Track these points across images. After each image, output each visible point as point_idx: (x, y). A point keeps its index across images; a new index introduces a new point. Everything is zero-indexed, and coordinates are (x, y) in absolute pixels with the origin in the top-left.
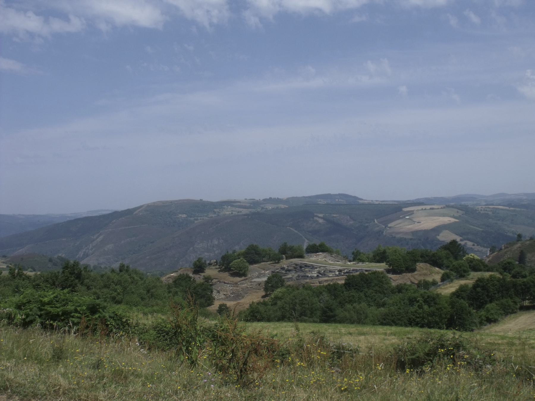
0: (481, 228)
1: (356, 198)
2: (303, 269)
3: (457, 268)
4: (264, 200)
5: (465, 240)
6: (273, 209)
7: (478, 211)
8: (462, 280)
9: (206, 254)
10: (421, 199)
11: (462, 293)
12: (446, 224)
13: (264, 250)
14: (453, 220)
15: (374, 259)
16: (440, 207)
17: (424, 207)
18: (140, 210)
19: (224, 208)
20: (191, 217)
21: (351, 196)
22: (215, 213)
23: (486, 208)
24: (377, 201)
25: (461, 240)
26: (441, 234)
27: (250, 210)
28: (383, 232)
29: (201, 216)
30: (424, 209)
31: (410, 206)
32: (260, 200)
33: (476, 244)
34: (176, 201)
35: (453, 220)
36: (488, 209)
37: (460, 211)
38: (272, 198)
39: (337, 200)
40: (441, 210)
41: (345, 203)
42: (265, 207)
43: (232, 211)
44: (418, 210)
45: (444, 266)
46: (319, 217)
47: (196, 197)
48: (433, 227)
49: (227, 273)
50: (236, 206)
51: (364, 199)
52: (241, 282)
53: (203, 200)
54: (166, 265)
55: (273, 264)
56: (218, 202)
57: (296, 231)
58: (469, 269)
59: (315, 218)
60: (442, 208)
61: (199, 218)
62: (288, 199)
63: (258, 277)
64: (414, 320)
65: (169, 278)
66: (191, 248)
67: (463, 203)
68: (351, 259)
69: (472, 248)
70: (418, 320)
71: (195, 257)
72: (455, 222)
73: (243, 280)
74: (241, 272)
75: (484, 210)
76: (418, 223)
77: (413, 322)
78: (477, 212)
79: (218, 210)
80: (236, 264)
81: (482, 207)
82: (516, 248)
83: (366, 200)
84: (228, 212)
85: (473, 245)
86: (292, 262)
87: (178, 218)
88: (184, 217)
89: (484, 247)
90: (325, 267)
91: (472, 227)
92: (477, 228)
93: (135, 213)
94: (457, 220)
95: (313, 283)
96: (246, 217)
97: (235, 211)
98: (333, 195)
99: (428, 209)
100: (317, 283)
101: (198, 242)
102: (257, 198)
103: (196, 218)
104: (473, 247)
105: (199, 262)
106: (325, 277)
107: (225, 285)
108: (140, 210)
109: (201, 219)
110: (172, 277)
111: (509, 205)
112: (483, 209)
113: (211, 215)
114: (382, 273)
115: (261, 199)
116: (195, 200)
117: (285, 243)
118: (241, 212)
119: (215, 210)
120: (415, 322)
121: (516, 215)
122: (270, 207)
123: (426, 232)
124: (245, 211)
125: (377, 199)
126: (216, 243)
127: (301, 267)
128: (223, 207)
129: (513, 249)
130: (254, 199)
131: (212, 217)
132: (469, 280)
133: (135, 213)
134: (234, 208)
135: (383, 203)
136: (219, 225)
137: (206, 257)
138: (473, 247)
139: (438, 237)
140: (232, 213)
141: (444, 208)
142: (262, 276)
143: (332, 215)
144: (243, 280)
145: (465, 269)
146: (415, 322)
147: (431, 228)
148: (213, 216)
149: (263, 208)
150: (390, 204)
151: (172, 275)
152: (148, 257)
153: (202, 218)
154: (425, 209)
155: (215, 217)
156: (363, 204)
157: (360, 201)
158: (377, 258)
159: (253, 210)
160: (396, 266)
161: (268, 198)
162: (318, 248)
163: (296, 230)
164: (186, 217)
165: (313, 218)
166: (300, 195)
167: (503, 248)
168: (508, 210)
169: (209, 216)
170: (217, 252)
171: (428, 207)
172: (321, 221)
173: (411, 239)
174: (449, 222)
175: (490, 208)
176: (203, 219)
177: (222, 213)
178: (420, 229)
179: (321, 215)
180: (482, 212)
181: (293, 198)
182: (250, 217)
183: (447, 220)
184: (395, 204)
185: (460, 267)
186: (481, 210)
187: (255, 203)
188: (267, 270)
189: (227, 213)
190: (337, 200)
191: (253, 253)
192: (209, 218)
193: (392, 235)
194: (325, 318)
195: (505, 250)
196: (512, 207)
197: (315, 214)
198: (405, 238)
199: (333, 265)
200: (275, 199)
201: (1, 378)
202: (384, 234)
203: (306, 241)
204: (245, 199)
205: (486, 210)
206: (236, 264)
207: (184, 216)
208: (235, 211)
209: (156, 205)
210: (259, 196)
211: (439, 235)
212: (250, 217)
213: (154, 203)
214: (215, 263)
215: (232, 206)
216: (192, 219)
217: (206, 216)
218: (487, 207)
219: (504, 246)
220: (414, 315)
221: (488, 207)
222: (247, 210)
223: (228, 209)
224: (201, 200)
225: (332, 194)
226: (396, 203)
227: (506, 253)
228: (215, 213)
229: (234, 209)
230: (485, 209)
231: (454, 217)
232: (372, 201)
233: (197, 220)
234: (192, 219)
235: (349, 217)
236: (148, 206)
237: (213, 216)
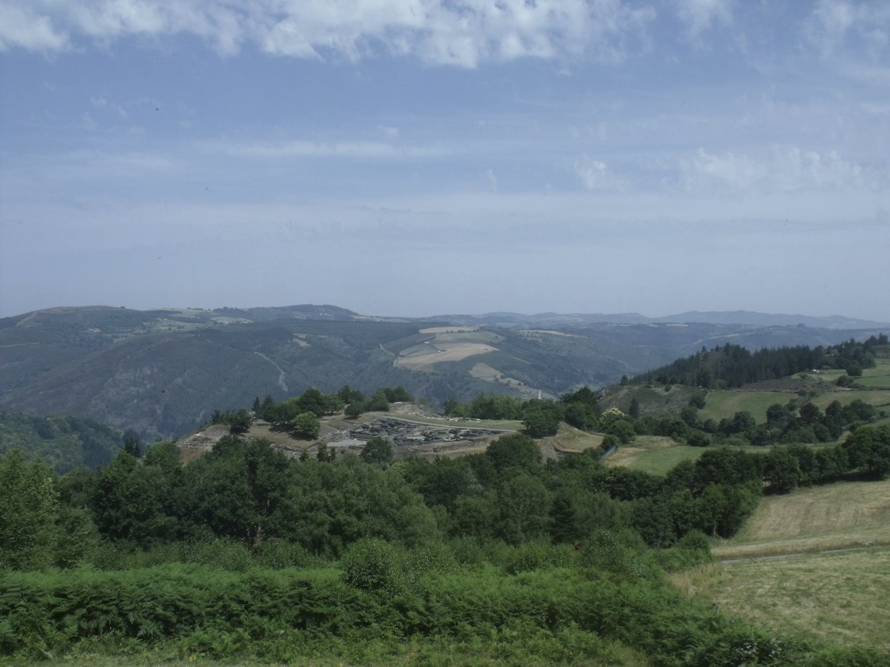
0: (528, 361)
1: (348, 312)
2: (395, 428)
3: (619, 430)
4: (217, 310)
5: (508, 377)
6: (232, 324)
7: (524, 336)
8: (626, 447)
9: (132, 388)
10: (439, 316)
11: (687, 471)
12: (481, 353)
13: (326, 398)
14: (490, 349)
15: (476, 413)
16: (471, 329)
17: (450, 329)
18: (26, 319)
19: (158, 321)
20: (107, 333)
21: (341, 309)
22: (144, 327)
23: (534, 332)
24: (378, 317)
25: (502, 377)
26: (474, 368)
27: (197, 325)
28: (392, 363)
29: (124, 332)
30: (449, 331)
31: (430, 327)
32: (209, 310)
33: (522, 384)
34: (85, 308)
35: (490, 349)
36: (537, 335)
37: (499, 336)
38: (227, 308)
39: (321, 314)
40: (474, 333)
41: (334, 319)
42: (219, 322)
43: (170, 325)
44: (441, 333)
45: (584, 425)
46: (300, 339)
47: (115, 302)
48: (463, 358)
49: (284, 433)
50: (176, 319)
51: (360, 314)
52: (311, 448)
53: (126, 308)
54: (70, 404)
55: (349, 421)
56: (147, 312)
57: (267, 359)
58: (634, 432)
59: (295, 340)
60: (474, 331)
61: (120, 335)
62: (251, 310)
63: (333, 440)
64: (681, 517)
65: (194, 440)
66: (110, 380)
67: (498, 324)
68: (443, 411)
69: (517, 389)
70: (689, 516)
71: (115, 393)
72: (493, 352)
73: (314, 445)
74: (311, 433)
75: (532, 337)
76: (442, 351)
77: (679, 519)
78: (523, 338)
79: (149, 324)
80: (303, 420)
81: (528, 332)
82: (622, 396)
83: (363, 316)
84: (164, 326)
85: (519, 384)
86: (374, 418)
87: (88, 334)
88: (97, 333)
89: (534, 387)
90: (427, 425)
91: (516, 359)
92: (523, 361)
93: (18, 324)
94: (496, 349)
95: (425, 451)
96: (193, 335)
97: (174, 326)
98: (315, 306)
99: (455, 332)
100: (431, 451)
101: (121, 370)
102: (206, 308)
103: (115, 334)
104: (518, 387)
105: (241, 416)
106: (439, 442)
107: (289, 452)
108: (26, 319)
109: (122, 337)
110: (199, 439)
111: (564, 329)
112: (530, 335)
113: (138, 330)
114: (517, 437)
115: (212, 309)
116: (113, 308)
117: (347, 387)
118: (183, 327)
119: (144, 323)
120: (683, 519)
121: (574, 344)
122: (226, 321)
123: (453, 363)
124: (189, 327)
125: (380, 316)
126: (148, 372)
127: (392, 426)
128: (157, 319)
129: (619, 397)
130: (201, 309)
131: (139, 334)
132: (635, 446)
133: (18, 324)
134: (172, 321)
135: (387, 320)
136: (153, 346)
137: (133, 393)
138: (518, 387)
139: (470, 372)
140: (170, 329)
141: (478, 331)
142: (337, 438)
143: (319, 336)
144: (314, 445)
145: (630, 431)
146: (683, 519)
147: (460, 359)
148: (142, 332)
149: (215, 323)
150: (396, 323)
151: (198, 435)
152: (41, 393)
153: (124, 335)
154: (452, 332)
155: (144, 334)
156: (359, 321)
157: (355, 317)
158: (481, 411)
159: (201, 326)
160: (538, 427)
161: (222, 307)
162: (393, 395)
163: (267, 356)
164: (100, 332)
165: (292, 340)
166: (267, 304)
167: (604, 394)
168: (563, 337)
169: (135, 332)
170: (148, 386)
171: (456, 329)
172: (303, 344)
173: (433, 374)
174: (485, 352)
175: (539, 333)
176: (126, 336)
177: (154, 329)
178: (445, 360)
179: (303, 336)
180: (529, 339)
181: (258, 309)
182: (199, 336)
183: (482, 349)
184: (404, 323)
185: (624, 429)
186: (528, 336)
187: (202, 317)
188: (343, 430)
189: (163, 328)
190: (321, 314)
191: (314, 403)
192: (134, 336)
193: (405, 368)
194: (562, 516)
195: (609, 398)
196: (570, 332)
197: (294, 334)
198: (425, 373)
199: (437, 423)
200: (232, 309)
201: (559, 660)
202: (394, 365)
203: (283, 373)
204: (188, 308)
205: (535, 336)
206: (303, 420)
207: (97, 330)
208: (174, 326)
209: (52, 312)
210: (209, 305)
211: (471, 370)
212: (199, 336)
213: (49, 310)
214: (254, 416)
215: (170, 318)
216: (109, 335)
217: (131, 332)
218: (535, 331)
219: (605, 392)
220: (680, 510)
221: (537, 333)
222: (191, 324)
223: (164, 322)
224: (122, 307)
225: (314, 304)
226: (406, 322)
227: (611, 402)
228: (144, 327)
229: (172, 322)
230: (533, 335)
231: (491, 344)
232: (371, 317)
233: (116, 337)
234: (109, 335)
235: (342, 340)
236: (40, 313)
237: (142, 332)
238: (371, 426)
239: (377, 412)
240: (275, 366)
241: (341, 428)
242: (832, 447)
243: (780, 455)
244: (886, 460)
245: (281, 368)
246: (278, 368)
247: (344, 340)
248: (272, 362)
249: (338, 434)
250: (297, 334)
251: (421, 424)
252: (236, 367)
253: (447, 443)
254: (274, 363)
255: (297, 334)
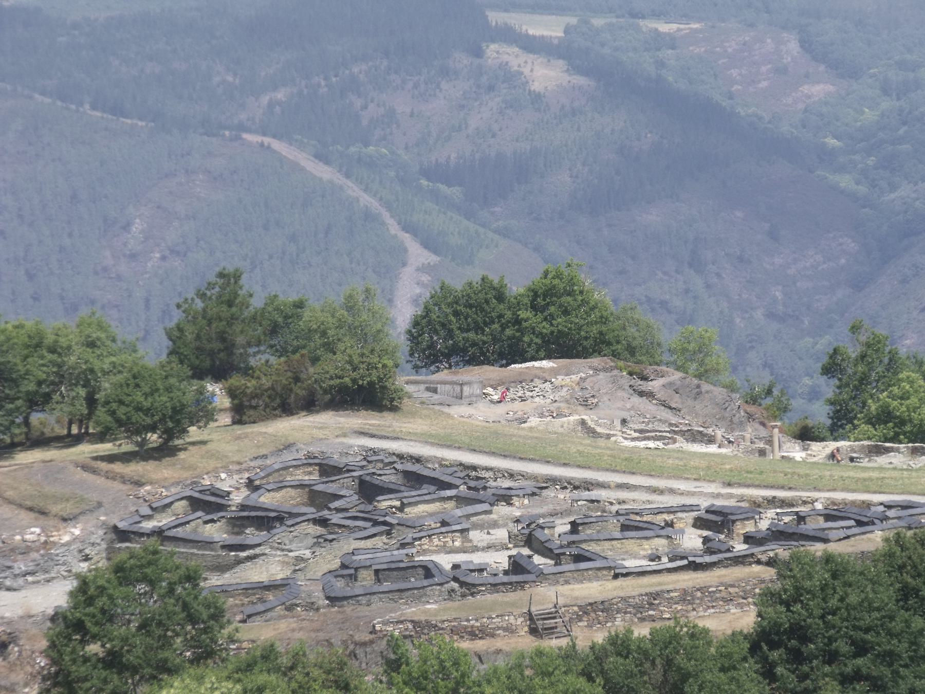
46: (531, 45)
55: (118, 467)
57: (325, 172)
90: (588, 485)
100: (510, 630)
106: (581, 577)
142: (21, 566)
165: (478, 53)
197: (495, 17)
203: (418, 255)
235: (793, 46)
238: (237, 498)
239: (327, 418)
240: (369, 216)
241: (55, 509)
242: (350, 192)
243: (330, 537)
244: (919, 581)
245: (406, 228)
246: (393, 228)
247: (806, 44)
248: (352, 189)
249: (26, 550)
250: (515, 19)
251: (553, 481)
252: (137, 226)
253: (646, 580)
254: (366, 200)
255: (515, 19)
